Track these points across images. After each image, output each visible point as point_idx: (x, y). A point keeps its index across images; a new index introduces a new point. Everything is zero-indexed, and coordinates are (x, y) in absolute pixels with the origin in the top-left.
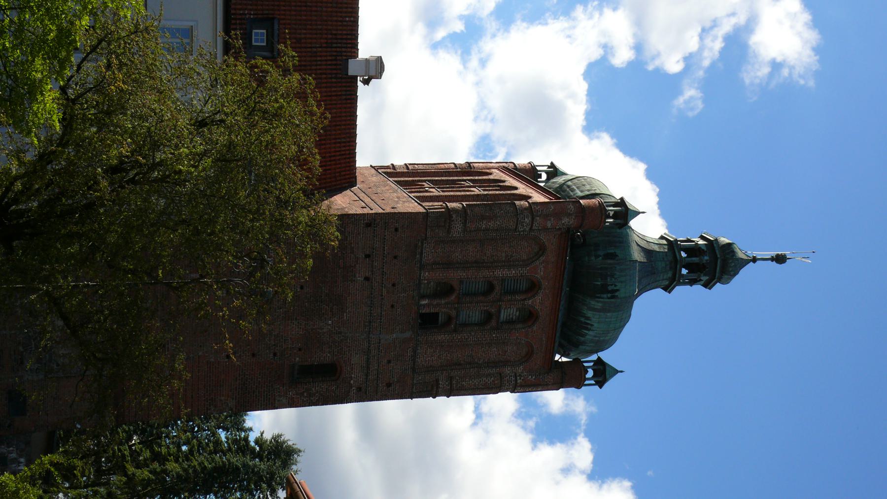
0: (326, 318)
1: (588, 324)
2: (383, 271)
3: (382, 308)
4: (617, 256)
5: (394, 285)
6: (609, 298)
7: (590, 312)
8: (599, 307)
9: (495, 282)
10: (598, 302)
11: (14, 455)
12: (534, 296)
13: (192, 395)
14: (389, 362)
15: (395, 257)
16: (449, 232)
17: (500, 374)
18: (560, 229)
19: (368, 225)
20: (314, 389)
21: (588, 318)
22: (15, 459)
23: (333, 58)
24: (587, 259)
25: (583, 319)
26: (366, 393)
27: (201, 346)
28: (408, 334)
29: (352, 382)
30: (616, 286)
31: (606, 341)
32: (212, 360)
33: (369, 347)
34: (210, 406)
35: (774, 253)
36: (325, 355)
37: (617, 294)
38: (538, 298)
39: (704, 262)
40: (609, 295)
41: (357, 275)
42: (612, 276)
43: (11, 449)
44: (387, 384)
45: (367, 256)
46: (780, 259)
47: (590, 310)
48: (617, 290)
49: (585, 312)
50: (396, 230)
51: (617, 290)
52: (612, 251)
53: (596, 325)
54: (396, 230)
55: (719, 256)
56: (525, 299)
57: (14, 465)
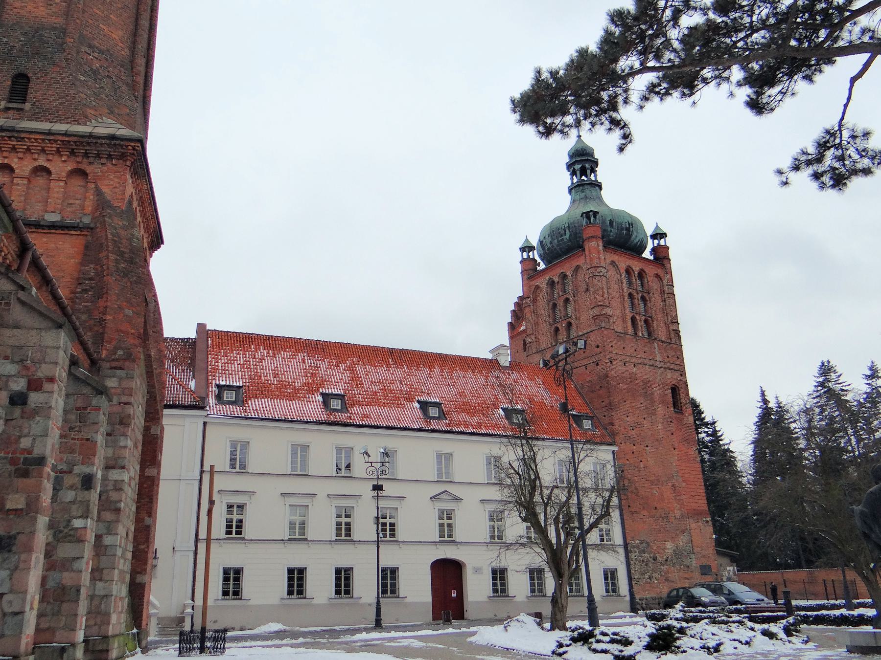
12: (633, 270)
14: (668, 357)
28: (656, 345)
50: (612, 346)
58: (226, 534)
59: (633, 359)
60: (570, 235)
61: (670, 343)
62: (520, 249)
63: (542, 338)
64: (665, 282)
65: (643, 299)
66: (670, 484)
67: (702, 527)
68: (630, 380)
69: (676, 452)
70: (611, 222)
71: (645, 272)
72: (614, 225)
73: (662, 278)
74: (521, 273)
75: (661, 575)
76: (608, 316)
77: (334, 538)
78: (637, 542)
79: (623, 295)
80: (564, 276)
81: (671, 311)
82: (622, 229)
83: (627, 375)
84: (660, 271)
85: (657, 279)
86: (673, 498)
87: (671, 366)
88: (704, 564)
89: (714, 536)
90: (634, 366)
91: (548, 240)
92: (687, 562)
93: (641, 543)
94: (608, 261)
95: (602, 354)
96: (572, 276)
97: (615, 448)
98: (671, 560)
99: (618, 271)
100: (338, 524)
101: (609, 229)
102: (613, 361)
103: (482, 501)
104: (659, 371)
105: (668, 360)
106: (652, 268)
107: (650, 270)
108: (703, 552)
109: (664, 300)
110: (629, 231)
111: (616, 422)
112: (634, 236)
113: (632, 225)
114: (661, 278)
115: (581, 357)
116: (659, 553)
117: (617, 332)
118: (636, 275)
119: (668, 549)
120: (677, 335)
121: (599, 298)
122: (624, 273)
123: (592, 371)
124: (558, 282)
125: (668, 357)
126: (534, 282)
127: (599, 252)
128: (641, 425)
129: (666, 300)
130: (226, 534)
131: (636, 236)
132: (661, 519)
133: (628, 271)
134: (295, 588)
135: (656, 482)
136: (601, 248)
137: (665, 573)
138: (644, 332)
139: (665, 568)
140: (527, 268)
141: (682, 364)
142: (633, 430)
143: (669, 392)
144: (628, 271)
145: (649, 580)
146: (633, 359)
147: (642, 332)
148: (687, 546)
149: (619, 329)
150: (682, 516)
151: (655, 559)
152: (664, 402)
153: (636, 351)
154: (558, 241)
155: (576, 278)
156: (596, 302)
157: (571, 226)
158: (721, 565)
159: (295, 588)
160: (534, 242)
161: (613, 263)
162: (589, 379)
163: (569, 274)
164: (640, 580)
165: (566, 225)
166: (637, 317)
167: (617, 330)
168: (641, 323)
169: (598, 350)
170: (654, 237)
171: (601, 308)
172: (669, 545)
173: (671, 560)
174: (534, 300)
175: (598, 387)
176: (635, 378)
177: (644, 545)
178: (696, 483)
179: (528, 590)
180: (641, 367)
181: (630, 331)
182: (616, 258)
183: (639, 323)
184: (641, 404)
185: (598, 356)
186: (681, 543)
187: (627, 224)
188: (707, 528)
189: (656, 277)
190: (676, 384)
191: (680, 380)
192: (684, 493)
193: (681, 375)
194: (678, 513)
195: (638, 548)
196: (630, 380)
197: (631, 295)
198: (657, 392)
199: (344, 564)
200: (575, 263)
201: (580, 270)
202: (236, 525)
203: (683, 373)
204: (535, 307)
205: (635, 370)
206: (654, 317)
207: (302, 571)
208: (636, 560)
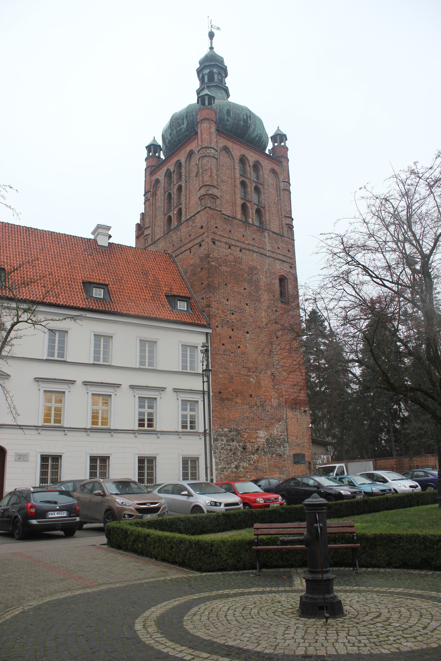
4: (228, 109)
14: (278, 248)
15: (230, 232)
21: (257, 135)
23: (99, 253)
24: (227, 127)
25: (257, 138)
28: (266, 234)
35: (208, 38)
37: (248, 115)
38: (249, 158)
40: (249, 119)
42: (239, 114)
46: (211, 35)
48: (246, 114)
50: (216, 227)
51: (246, 114)
52: (226, 111)
55: (215, 63)
56: (249, 165)
58: (139, 427)
59: (240, 244)
60: (188, 124)
61: (282, 236)
62: (146, 147)
63: (157, 230)
64: (281, 179)
65: (257, 190)
66: (269, 372)
67: (299, 416)
68: (234, 264)
70: (228, 112)
71: (260, 165)
72: (231, 114)
73: (279, 174)
74: (146, 170)
75: (250, 464)
76: (214, 197)
77: (137, 428)
78: (226, 430)
79: (235, 181)
80: (179, 165)
81: (285, 206)
82: (239, 120)
83: (231, 258)
84: (276, 168)
85: (273, 175)
86: (271, 386)
87: (280, 257)
89: (310, 425)
90: (241, 250)
91: (168, 133)
92: (280, 450)
93: (229, 431)
94: (221, 145)
95: (205, 235)
96: (186, 161)
97: (210, 331)
98: (263, 449)
99: (231, 157)
100: (184, 416)
101: (226, 117)
102: (216, 242)
103: (38, 380)
104: (268, 260)
105: (278, 251)
106: (268, 163)
107: (266, 165)
109: (279, 195)
110: (247, 123)
111: (214, 304)
112: (251, 129)
113: (250, 117)
114: (277, 174)
115: (187, 241)
116: (250, 442)
117: (223, 214)
118: (251, 165)
119: (261, 438)
120: (290, 230)
121: (206, 178)
122: (237, 161)
123: (195, 254)
124: (174, 171)
125: (278, 248)
126: (155, 176)
127: (210, 133)
129: (281, 195)
130: (139, 427)
131: (254, 130)
132: (256, 407)
133: (243, 160)
135: (254, 370)
136: (213, 130)
137: (254, 462)
138: (254, 221)
139: (255, 457)
140: (150, 165)
141: (293, 257)
142: (233, 314)
144: (243, 160)
145: (235, 470)
146: (240, 244)
147: (253, 218)
148: (281, 435)
149: (228, 212)
150: (279, 405)
151: (244, 448)
152: (270, 291)
153: (243, 236)
154: (177, 132)
155: (189, 165)
156: (203, 182)
157: (188, 115)
158: (315, 454)
160: (160, 142)
161: (226, 149)
162: (191, 262)
163: (183, 161)
164: (225, 470)
165: (184, 115)
166: (249, 205)
167: (223, 212)
168: (252, 212)
169: (202, 231)
170: (274, 138)
171: (208, 188)
172: (262, 434)
173: (263, 449)
174: (153, 194)
175: (199, 270)
176: (240, 263)
177: (233, 433)
179: (179, 469)
180: (248, 252)
181: (239, 216)
182: (230, 144)
183: (250, 211)
184: (245, 289)
185: (201, 237)
186: (275, 432)
187: (245, 116)
188: (305, 417)
189: (273, 173)
190: (285, 275)
191: (290, 272)
193: (291, 267)
194: (275, 402)
195: (226, 436)
196: (234, 264)
197: (243, 184)
198: (263, 280)
200: (188, 149)
201: (193, 156)
203: (293, 266)
204: (154, 201)
205: (240, 255)
206: (267, 208)
208: (223, 448)
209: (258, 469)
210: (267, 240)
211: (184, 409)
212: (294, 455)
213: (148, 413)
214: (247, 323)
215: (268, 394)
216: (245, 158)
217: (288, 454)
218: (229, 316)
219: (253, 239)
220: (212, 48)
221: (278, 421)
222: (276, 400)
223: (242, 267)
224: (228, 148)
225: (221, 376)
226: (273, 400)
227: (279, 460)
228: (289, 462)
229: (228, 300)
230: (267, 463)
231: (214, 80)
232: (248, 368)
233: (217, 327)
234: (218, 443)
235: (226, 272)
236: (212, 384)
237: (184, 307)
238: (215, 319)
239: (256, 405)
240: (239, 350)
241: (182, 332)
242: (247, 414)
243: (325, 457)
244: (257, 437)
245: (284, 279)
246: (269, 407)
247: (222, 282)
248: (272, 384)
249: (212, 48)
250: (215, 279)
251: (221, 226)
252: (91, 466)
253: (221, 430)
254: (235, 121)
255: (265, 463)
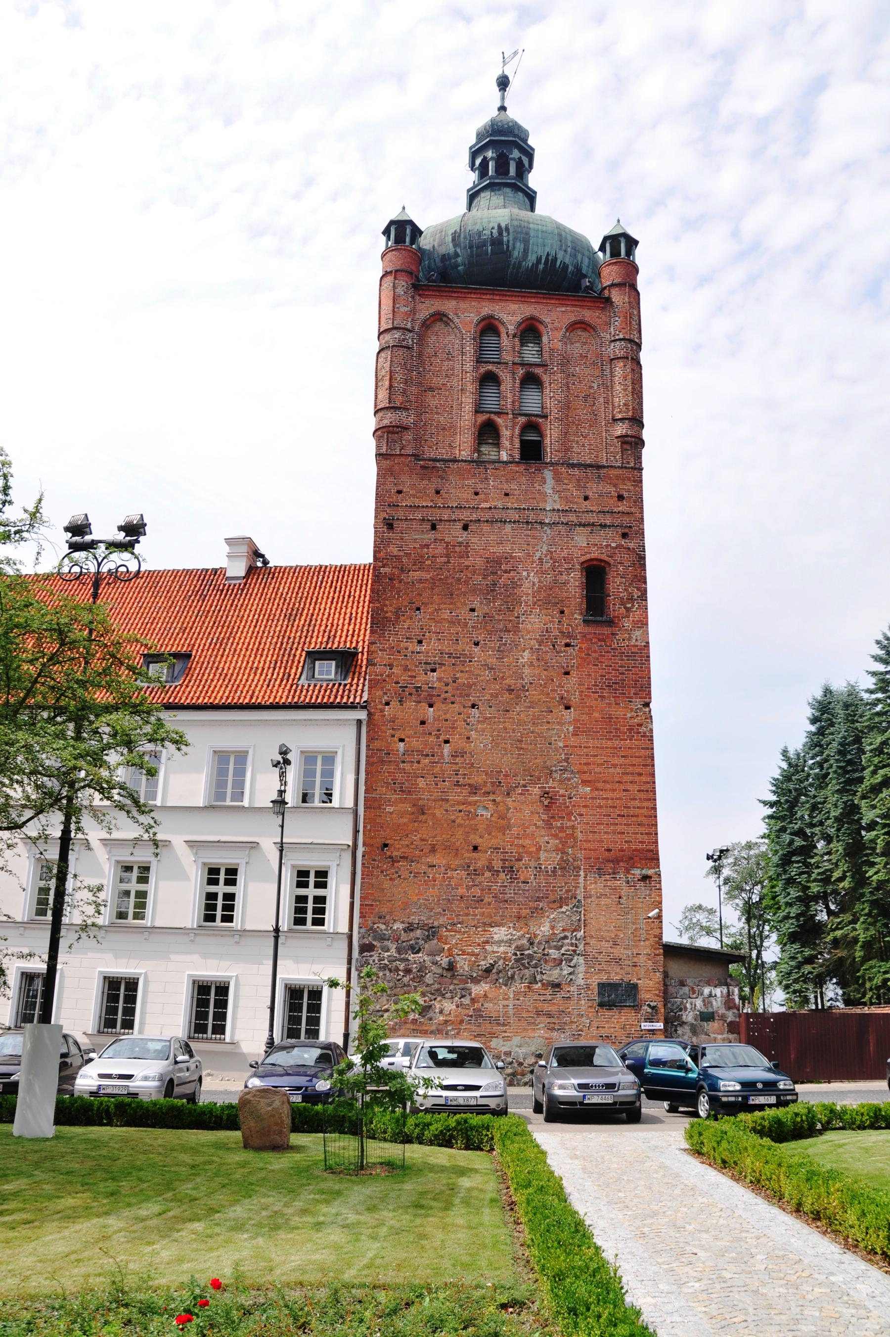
0: (519, 579)
1: (547, 259)
2: (457, 507)
3: (508, 508)
5: (477, 494)
6: (509, 234)
7: (529, 258)
8: (522, 246)
9: (482, 370)
10: (514, 248)
11: (699, 1003)
12: (503, 323)
13: (622, 757)
15: (438, 492)
16: (406, 428)
17: (612, 360)
18: (413, 297)
19: (390, 526)
20: (621, 595)
21: (539, 260)
22: (704, 1001)
25: (541, 267)
26: (630, 527)
27: (550, 744)
29: (613, 545)
30: (493, 228)
31: (578, 245)
32: (571, 729)
33: (562, 523)
34: (640, 733)
36: (572, 580)
38: (505, 318)
39: (494, 155)
41: (460, 539)
43: (688, 1005)
44: (619, 500)
45: (434, 527)
46: (503, 83)
47: (527, 256)
49: (530, 264)
50: (399, 492)
53: (547, 249)
54: (399, 492)
57: (714, 1003)
66: (536, 791)
69: (569, 715)
71: (541, 322)
86: (540, 823)
88: (615, 978)
100: (212, 896)
108: (618, 952)
128: (460, 659)
132: (488, 874)
134: (210, 1022)
135: (489, 787)
142: (433, 670)
143: (574, 582)
159: (210, 1022)
166: (499, 421)
178: (630, 787)
179: (235, 1007)
180: (486, 528)
184: (473, 610)
192: (583, 811)
194: (549, 859)
196: (444, 559)
199: (121, 968)
202: (306, 913)
207: (132, 985)
209: (481, 1016)
210: (548, 488)
211: (213, 882)
212: (601, 986)
213: (137, 892)
214: (474, 684)
215: (527, 842)
216: (497, 323)
217: (582, 982)
218: (422, 677)
219: (507, 495)
220: (503, 108)
221: (554, 906)
222: (554, 855)
223: (466, 563)
224: (445, 316)
225: (391, 809)
226: (543, 855)
227: (550, 997)
228: (583, 1002)
229: (420, 642)
230: (511, 1003)
231: (509, 173)
232: (470, 785)
233: (387, 704)
234: (371, 956)
235: (420, 581)
236: (365, 827)
237: (329, 673)
238: (382, 688)
239: (490, 868)
240: (447, 749)
241: (251, 725)
242: (461, 891)
243: (718, 991)
244: (487, 942)
245: (604, 568)
246: (531, 872)
247: (406, 606)
248: (545, 817)
249: (503, 108)
250: (387, 602)
251: (412, 486)
252: (224, 1019)
253: (383, 927)
254: (472, 252)
255: (505, 1003)
